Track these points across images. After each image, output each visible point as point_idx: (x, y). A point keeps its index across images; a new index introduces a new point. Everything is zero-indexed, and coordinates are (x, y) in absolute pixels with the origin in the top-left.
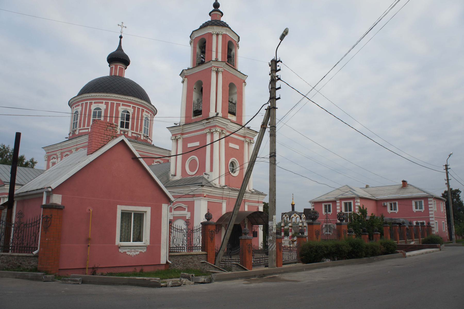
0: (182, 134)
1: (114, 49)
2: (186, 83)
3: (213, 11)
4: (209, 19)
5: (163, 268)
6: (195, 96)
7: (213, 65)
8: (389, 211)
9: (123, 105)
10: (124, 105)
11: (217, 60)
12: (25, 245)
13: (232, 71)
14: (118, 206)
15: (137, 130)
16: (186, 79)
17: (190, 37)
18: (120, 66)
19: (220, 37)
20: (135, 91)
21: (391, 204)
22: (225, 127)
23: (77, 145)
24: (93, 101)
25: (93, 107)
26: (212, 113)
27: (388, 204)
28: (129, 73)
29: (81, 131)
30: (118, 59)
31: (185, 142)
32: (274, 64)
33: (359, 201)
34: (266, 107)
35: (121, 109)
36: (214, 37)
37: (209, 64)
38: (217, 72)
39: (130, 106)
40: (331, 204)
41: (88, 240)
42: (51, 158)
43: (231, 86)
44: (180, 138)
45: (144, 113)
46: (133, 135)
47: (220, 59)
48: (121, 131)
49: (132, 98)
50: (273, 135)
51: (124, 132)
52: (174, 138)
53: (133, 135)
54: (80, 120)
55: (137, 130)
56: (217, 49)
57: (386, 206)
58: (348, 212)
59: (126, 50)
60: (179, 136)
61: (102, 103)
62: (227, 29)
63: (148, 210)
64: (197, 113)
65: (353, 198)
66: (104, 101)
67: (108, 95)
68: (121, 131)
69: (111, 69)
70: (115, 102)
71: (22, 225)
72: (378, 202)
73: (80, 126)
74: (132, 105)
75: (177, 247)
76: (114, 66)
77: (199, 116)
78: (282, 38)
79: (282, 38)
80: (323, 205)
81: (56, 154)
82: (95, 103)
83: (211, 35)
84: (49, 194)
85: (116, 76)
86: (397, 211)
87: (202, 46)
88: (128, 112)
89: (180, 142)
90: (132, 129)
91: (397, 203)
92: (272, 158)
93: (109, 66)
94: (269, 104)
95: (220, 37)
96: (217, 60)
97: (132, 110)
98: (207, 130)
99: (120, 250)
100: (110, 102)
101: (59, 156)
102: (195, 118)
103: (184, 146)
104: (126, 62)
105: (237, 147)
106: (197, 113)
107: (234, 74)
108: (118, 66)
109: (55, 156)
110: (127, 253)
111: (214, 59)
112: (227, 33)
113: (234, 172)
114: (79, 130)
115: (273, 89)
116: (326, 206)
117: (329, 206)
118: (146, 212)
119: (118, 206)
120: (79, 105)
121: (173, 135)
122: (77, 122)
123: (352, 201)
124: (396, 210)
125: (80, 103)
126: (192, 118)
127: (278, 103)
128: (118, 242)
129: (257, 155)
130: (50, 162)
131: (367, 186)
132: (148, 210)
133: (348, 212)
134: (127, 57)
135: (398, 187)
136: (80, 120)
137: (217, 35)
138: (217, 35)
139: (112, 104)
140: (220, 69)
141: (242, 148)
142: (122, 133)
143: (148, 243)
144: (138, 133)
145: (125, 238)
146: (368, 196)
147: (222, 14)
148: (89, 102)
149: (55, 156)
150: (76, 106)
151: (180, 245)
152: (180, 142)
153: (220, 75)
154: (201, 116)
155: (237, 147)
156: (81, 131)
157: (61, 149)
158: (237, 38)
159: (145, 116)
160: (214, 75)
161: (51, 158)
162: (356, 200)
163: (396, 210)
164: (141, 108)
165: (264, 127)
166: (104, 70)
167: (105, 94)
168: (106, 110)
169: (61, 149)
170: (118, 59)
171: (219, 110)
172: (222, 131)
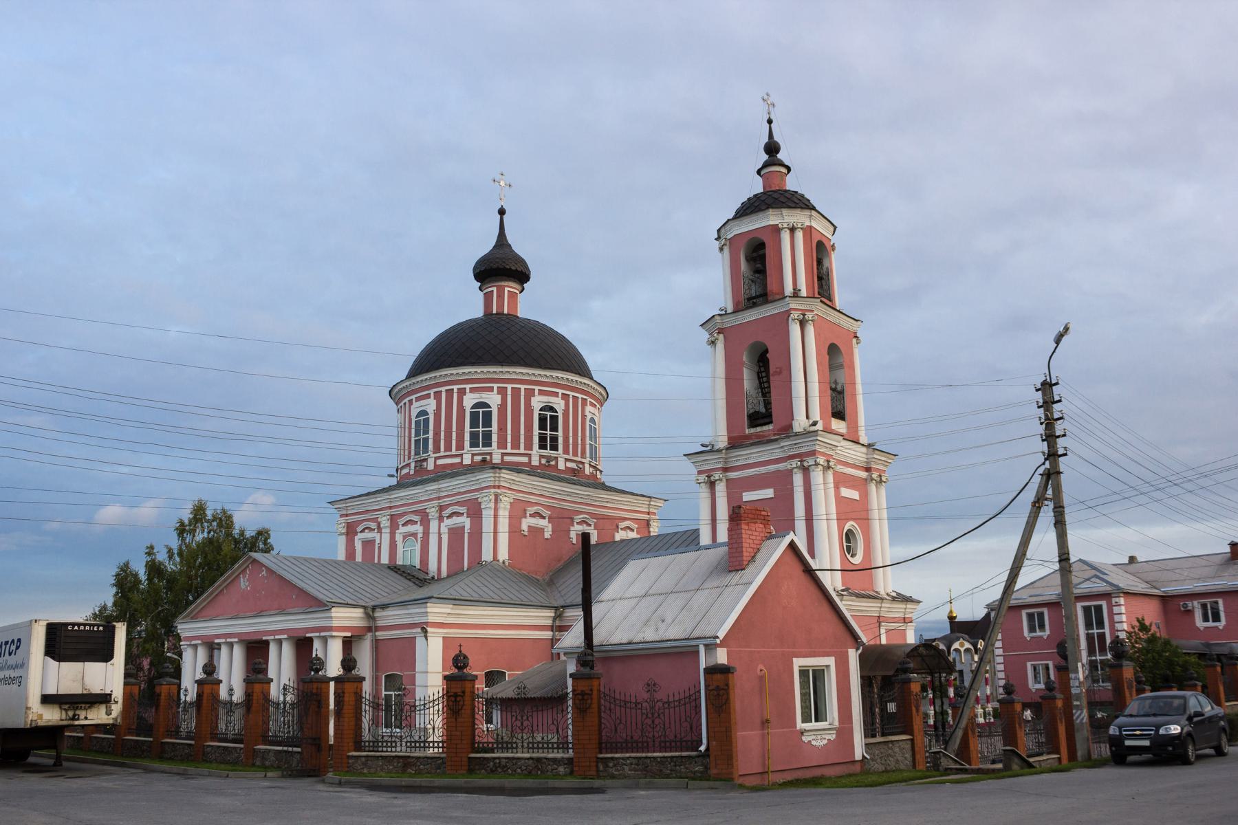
0: (725, 470)
1: (486, 245)
2: (720, 345)
3: (766, 165)
4: (757, 187)
5: (857, 768)
6: (748, 382)
7: (792, 306)
8: (1200, 623)
9: (541, 393)
10: (542, 390)
11: (796, 294)
12: (672, 737)
13: (833, 316)
14: (795, 660)
15: (575, 454)
16: (721, 336)
17: (719, 231)
18: (510, 287)
19: (799, 235)
20: (549, 352)
21: (1204, 606)
22: (831, 453)
23: (439, 498)
24: (468, 387)
25: (469, 400)
26: (800, 422)
27: (1196, 605)
28: (530, 304)
29: (440, 462)
30: (500, 268)
31: (735, 488)
32: (1047, 386)
33: (1122, 601)
34: (1041, 470)
35: (537, 402)
36: (785, 236)
37: (781, 303)
38: (803, 323)
39: (556, 394)
40: (1045, 611)
41: (765, 723)
42: (359, 529)
43: (833, 350)
44: (720, 480)
45: (589, 408)
46: (570, 465)
47: (804, 293)
48: (541, 457)
49: (560, 374)
50: (1060, 524)
51: (549, 459)
52: (703, 478)
53: (570, 465)
54: (437, 434)
55: (575, 454)
56: (793, 267)
57: (1190, 613)
58: (1095, 631)
59: (520, 245)
60: (717, 476)
61: (491, 389)
62: (813, 213)
63: (830, 661)
64: (758, 419)
65: (1107, 596)
66: (495, 386)
67: (505, 369)
68: (541, 457)
69: (488, 298)
70: (523, 387)
71: (660, 704)
72: (1170, 603)
73: (437, 449)
74: (561, 391)
75: (626, 742)
76: (494, 289)
77: (765, 428)
78: (1058, 340)
79: (1058, 340)
80: (1024, 613)
81: (375, 520)
82: (473, 390)
83: (776, 230)
84: (710, 648)
85: (500, 314)
86: (1222, 624)
87: (755, 262)
88: (552, 409)
89: (721, 488)
90: (566, 451)
91: (1220, 602)
92: (1064, 563)
93: (480, 289)
94: (1047, 465)
95: (799, 235)
96: (796, 294)
97: (563, 403)
98: (795, 463)
99: (804, 738)
100: (509, 387)
101: (385, 522)
102: (752, 430)
103: (733, 496)
104: (521, 275)
105: (855, 495)
106: (758, 419)
107: (837, 321)
108: (507, 289)
109: (373, 525)
110: (814, 743)
111: (789, 289)
112: (814, 224)
113: (852, 556)
114: (436, 458)
115: (1050, 437)
116: (1031, 616)
117: (1041, 615)
118: (828, 666)
119: (795, 660)
120: (428, 396)
121: (700, 473)
122: (426, 440)
123: (1104, 603)
124: (1219, 620)
125: (432, 392)
126: (747, 431)
127: (1063, 463)
128: (800, 725)
129: (1025, 555)
130: (356, 538)
131: (1132, 560)
132: (830, 661)
133: (1095, 631)
134: (522, 261)
135: (1218, 559)
136: (437, 434)
137: (792, 230)
138: (792, 230)
139: (516, 392)
140: (809, 316)
141: (865, 495)
142: (544, 461)
143: (836, 723)
144: (579, 459)
145: (806, 719)
146: (1141, 587)
147: (789, 169)
148: (455, 388)
149: (373, 525)
150: (418, 399)
151: (506, 739)
152: (721, 488)
153: (810, 330)
154: (771, 427)
155: (855, 495)
156: (440, 462)
157: (390, 508)
158: (832, 229)
159: (589, 416)
160: (795, 329)
161: (359, 529)
162: (1114, 600)
163: (1219, 620)
164: (580, 396)
165: (1037, 505)
166: (468, 303)
167: (498, 369)
168: (502, 409)
169: (390, 508)
170: (500, 268)
171: (816, 415)
172: (828, 461)
